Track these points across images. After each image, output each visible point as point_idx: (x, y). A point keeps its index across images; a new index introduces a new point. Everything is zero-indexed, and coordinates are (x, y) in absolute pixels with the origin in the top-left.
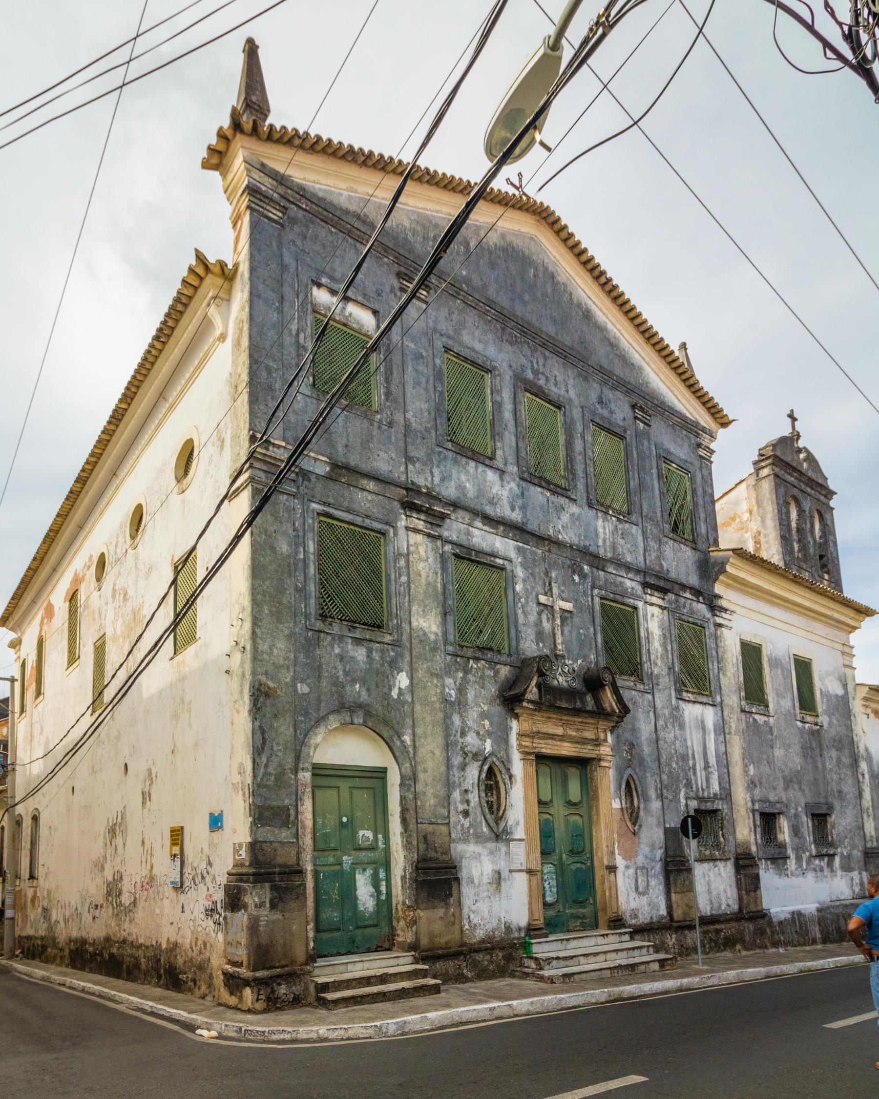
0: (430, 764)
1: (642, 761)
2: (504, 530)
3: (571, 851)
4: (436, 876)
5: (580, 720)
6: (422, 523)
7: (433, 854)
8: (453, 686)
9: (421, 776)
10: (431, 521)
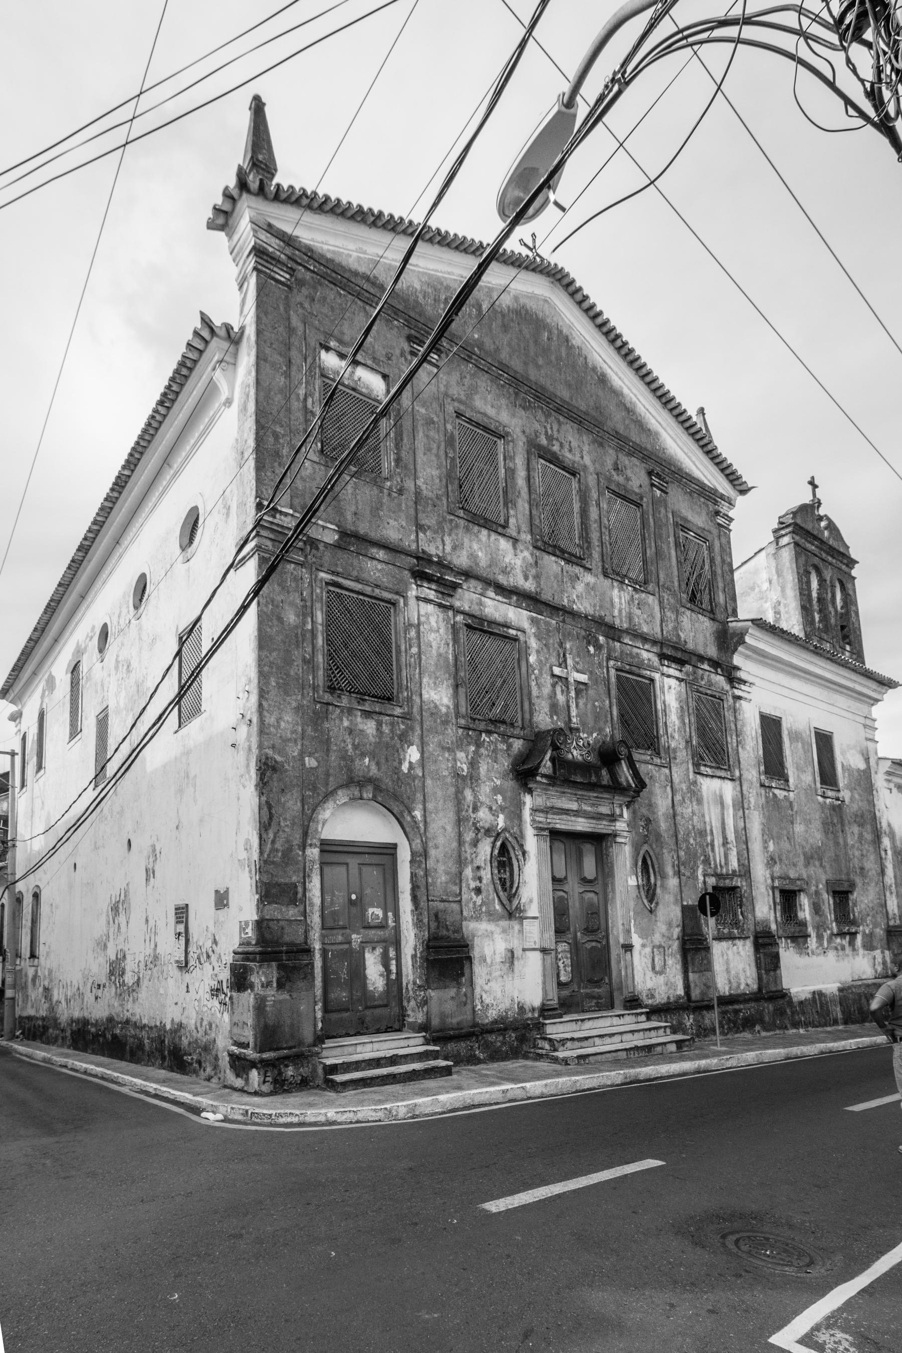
0: (441, 840)
2: (518, 600)
5: (595, 795)
6: (433, 592)
7: (445, 932)
8: (465, 760)
9: (432, 852)
10: (443, 590)
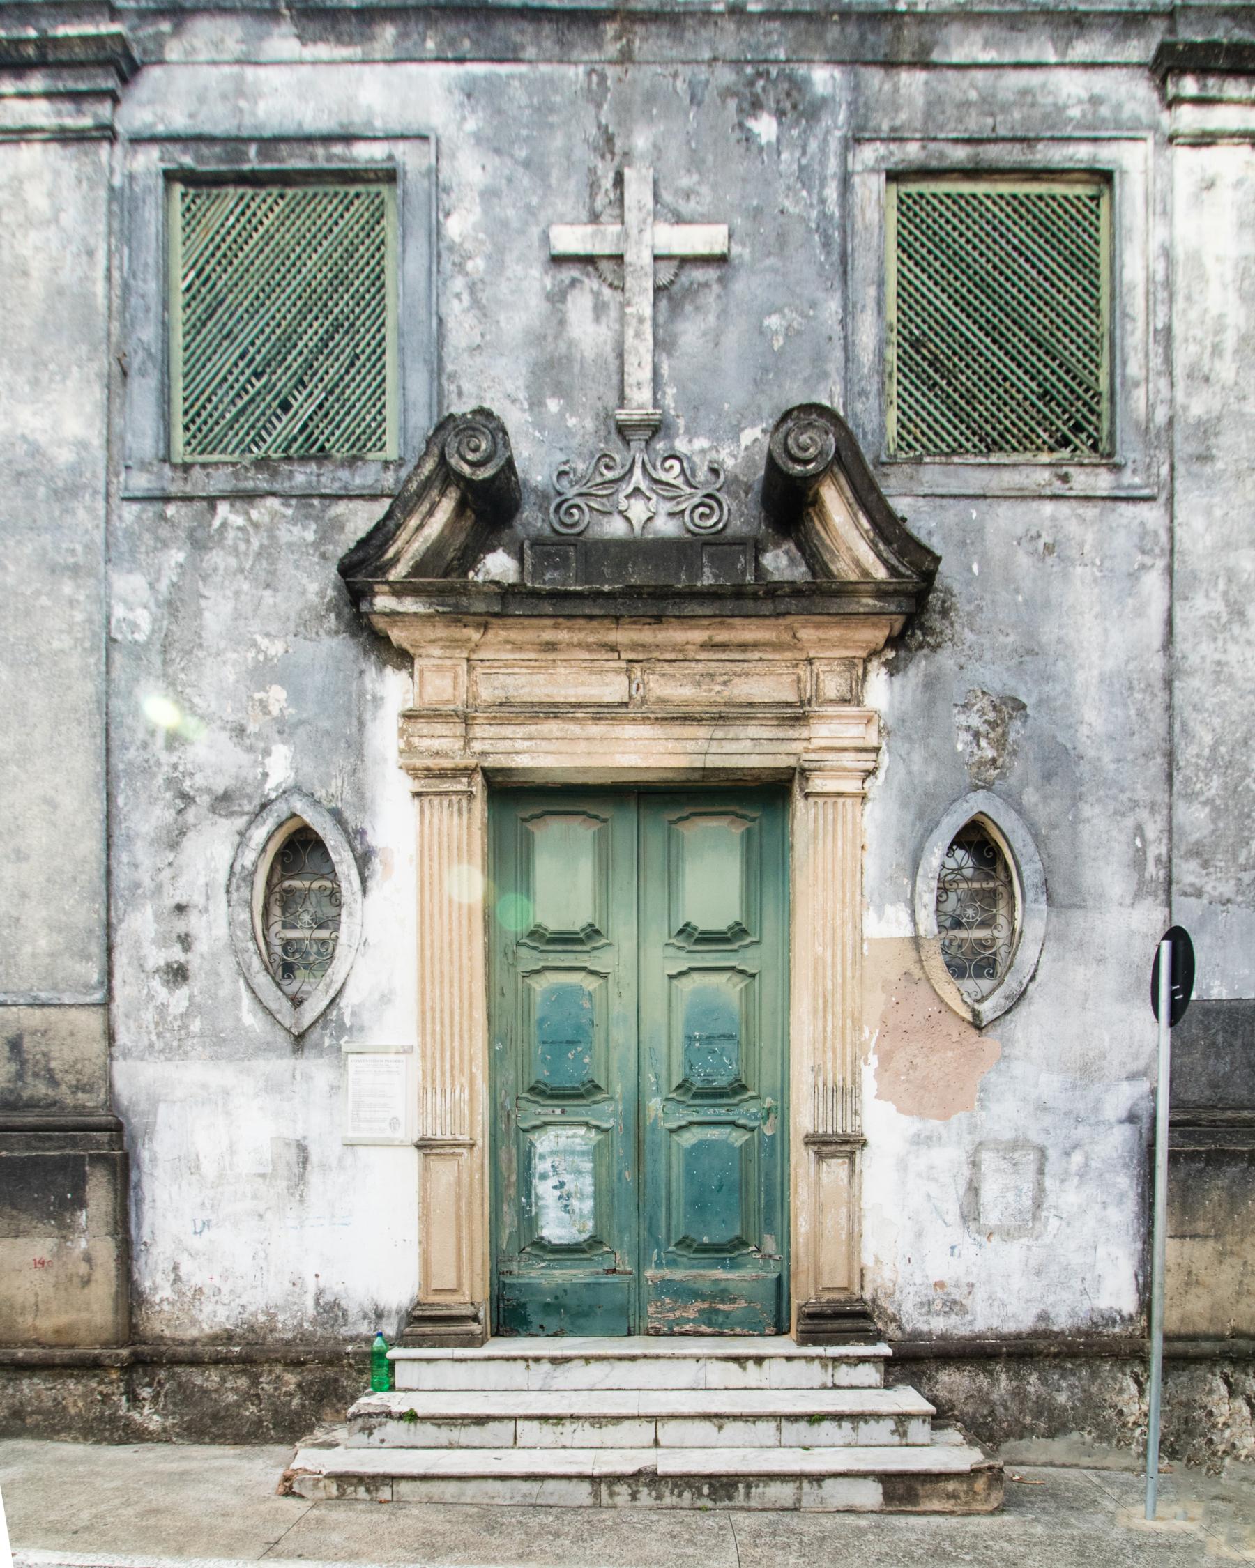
1: (1059, 763)
2: (403, 35)
3: (683, 1086)
4: (29, 1147)
5: (699, 636)
6: (42, 105)
7: (41, 1089)
8: (145, 594)
10: (71, 85)
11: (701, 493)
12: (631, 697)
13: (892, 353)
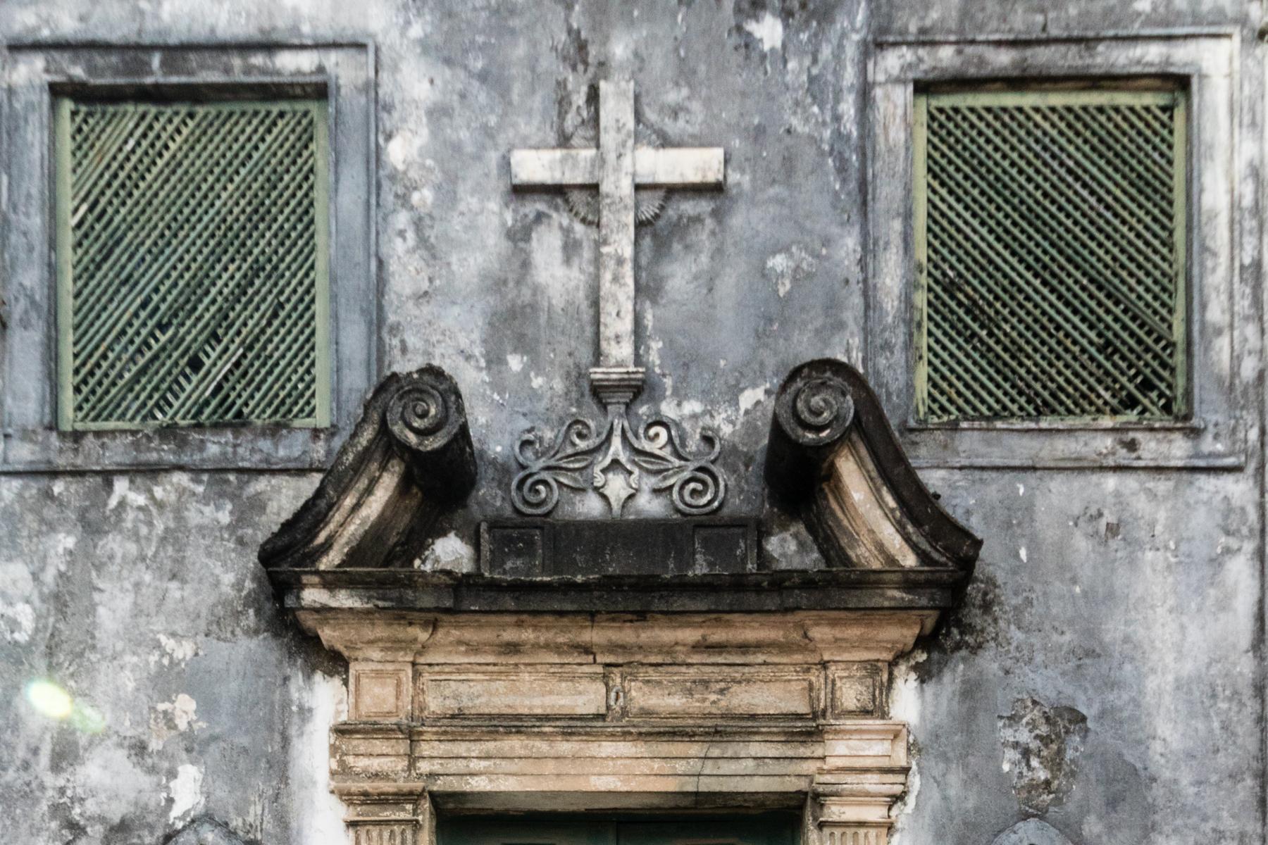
5: (690, 635)
8: (27, 586)
11: (692, 466)
12: (608, 707)
13: (921, 299)
